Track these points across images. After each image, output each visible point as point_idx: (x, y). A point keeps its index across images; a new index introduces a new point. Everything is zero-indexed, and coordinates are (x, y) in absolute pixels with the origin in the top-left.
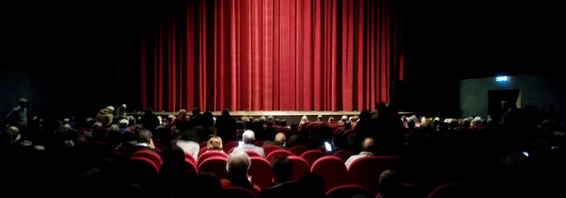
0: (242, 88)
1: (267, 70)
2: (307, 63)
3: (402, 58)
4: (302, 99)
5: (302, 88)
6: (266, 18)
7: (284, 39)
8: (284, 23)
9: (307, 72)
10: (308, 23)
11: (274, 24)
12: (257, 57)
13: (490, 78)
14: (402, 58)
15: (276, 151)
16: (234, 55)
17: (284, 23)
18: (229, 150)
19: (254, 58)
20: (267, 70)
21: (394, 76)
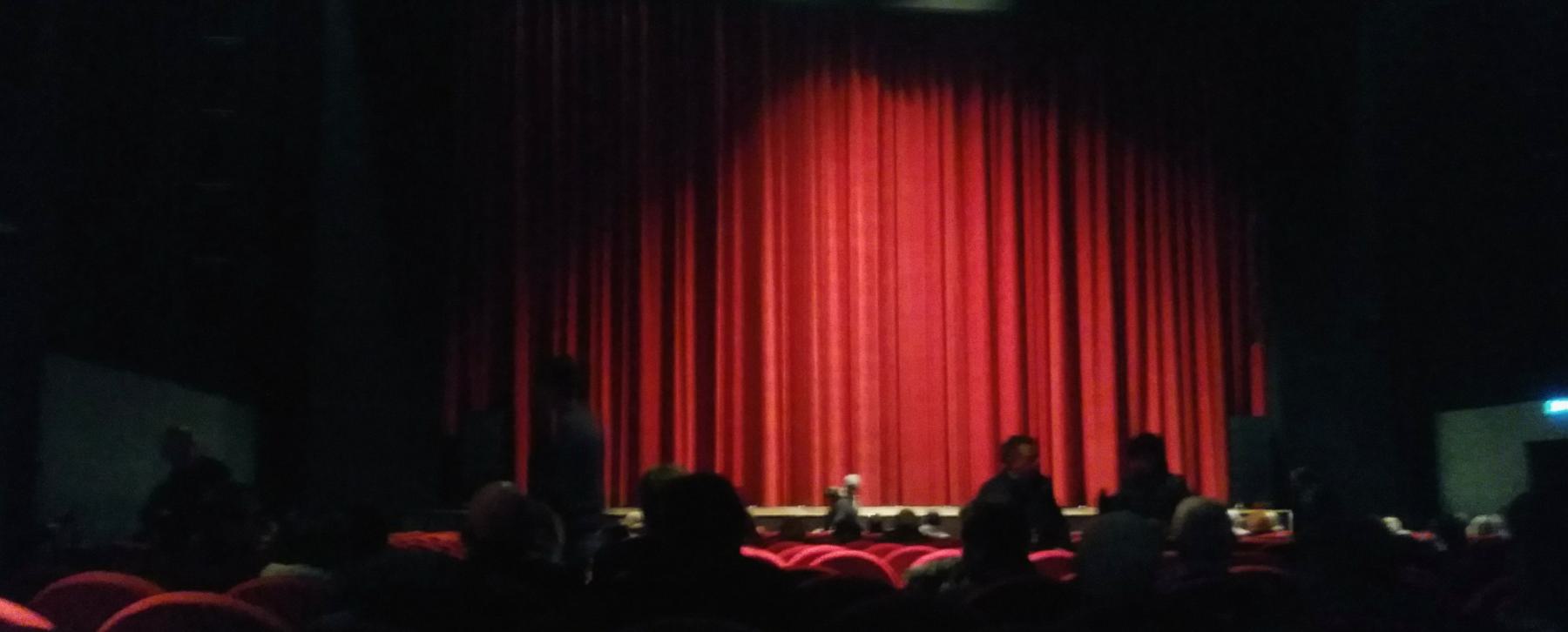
0: (793, 407)
1: (864, 386)
2: (979, 368)
3: (1257, 349)
4: (948, 490)
5: (1141, 250)
6: (860, 243)
7: (910, 302)
8: (909, 261)
9: (980, 393)
10: (978, 254)
11: (883, 263)
12: (835, 353)
13: (1524, 406)
14: (1257, 349)
15: (136, 607)
16: (771, 396)
17: (909, 261)
18: (84, 571)
19: (827, 355)
20: (864, 386)
21: (1236, 403)
